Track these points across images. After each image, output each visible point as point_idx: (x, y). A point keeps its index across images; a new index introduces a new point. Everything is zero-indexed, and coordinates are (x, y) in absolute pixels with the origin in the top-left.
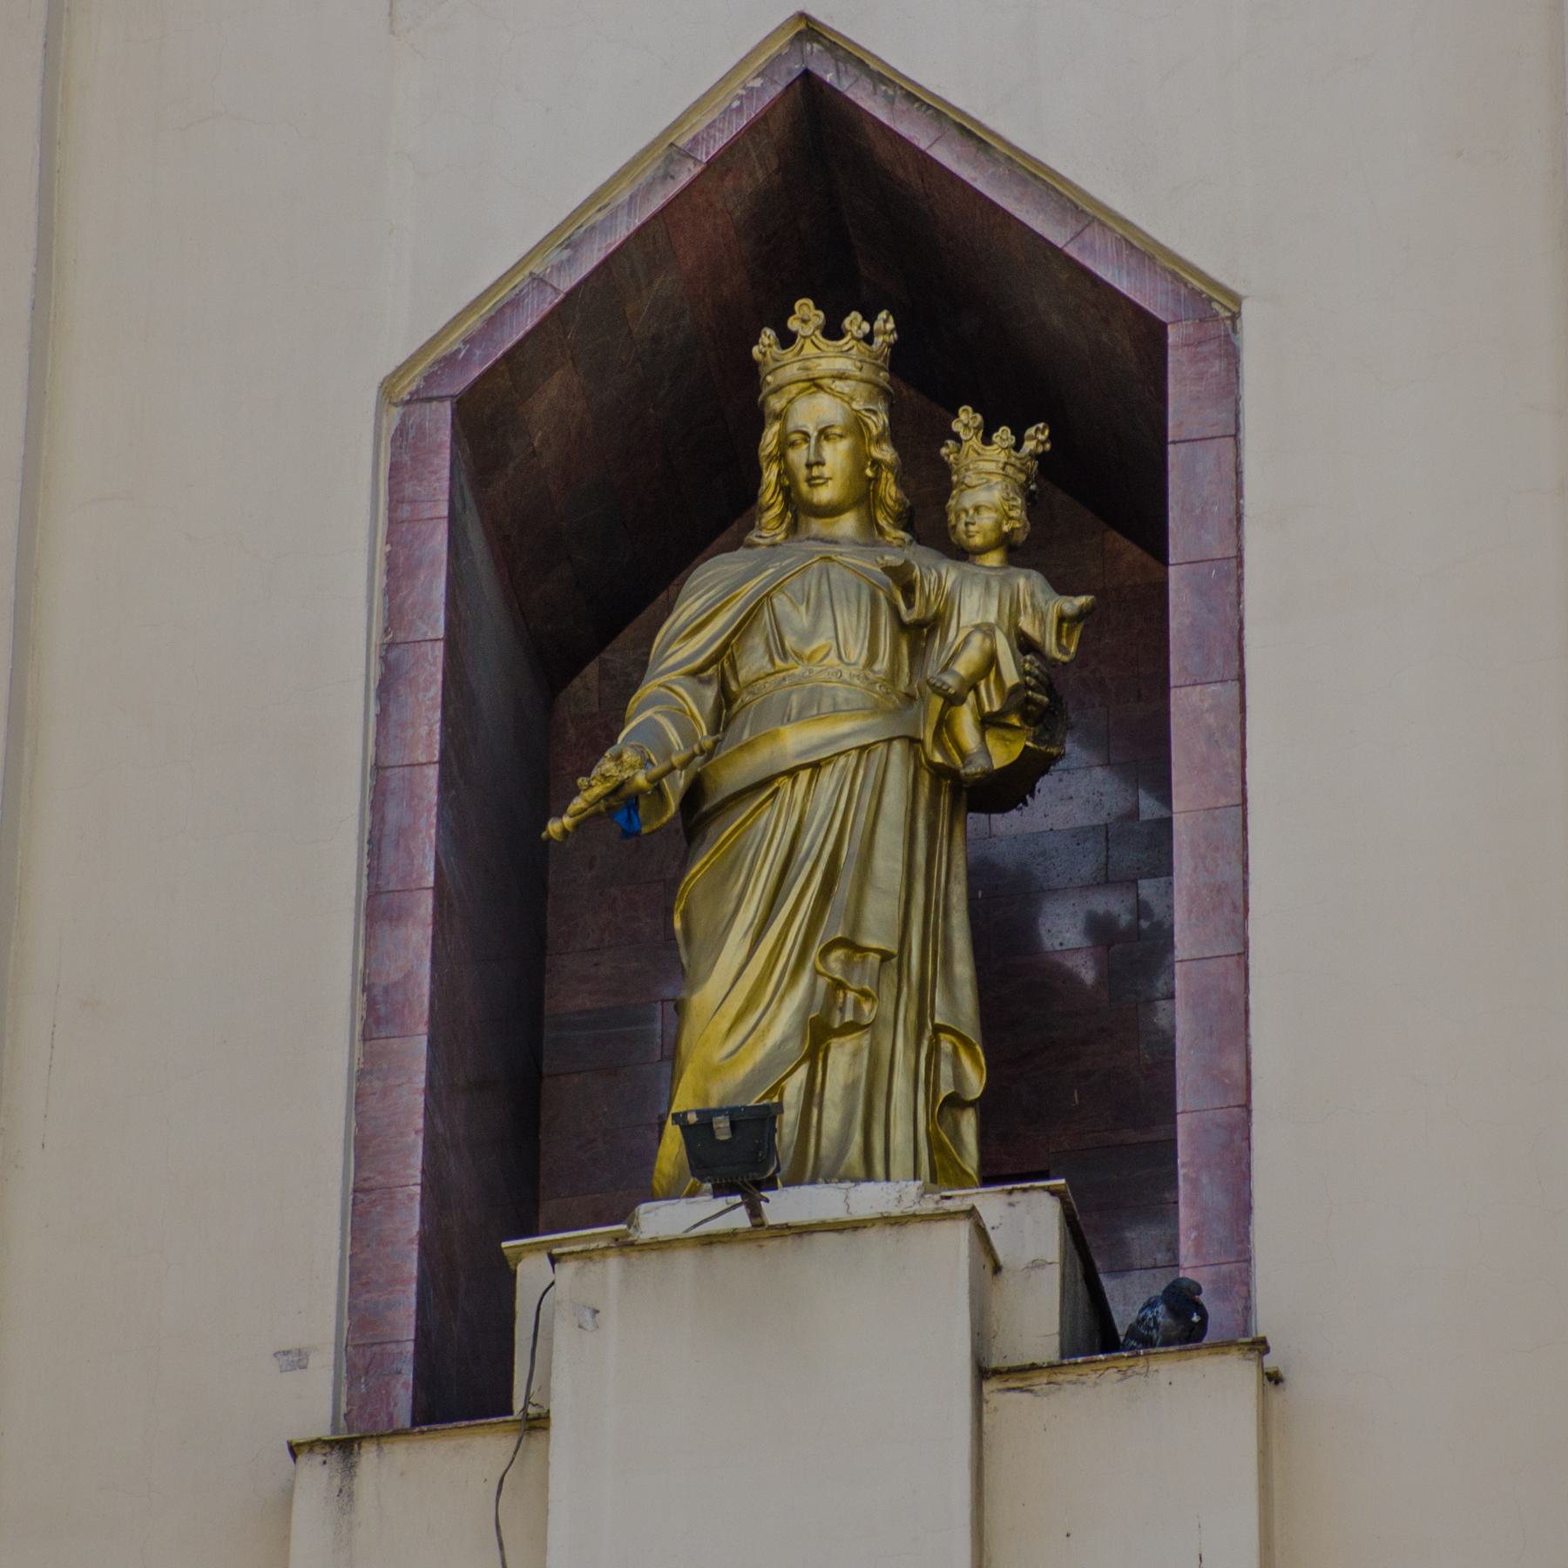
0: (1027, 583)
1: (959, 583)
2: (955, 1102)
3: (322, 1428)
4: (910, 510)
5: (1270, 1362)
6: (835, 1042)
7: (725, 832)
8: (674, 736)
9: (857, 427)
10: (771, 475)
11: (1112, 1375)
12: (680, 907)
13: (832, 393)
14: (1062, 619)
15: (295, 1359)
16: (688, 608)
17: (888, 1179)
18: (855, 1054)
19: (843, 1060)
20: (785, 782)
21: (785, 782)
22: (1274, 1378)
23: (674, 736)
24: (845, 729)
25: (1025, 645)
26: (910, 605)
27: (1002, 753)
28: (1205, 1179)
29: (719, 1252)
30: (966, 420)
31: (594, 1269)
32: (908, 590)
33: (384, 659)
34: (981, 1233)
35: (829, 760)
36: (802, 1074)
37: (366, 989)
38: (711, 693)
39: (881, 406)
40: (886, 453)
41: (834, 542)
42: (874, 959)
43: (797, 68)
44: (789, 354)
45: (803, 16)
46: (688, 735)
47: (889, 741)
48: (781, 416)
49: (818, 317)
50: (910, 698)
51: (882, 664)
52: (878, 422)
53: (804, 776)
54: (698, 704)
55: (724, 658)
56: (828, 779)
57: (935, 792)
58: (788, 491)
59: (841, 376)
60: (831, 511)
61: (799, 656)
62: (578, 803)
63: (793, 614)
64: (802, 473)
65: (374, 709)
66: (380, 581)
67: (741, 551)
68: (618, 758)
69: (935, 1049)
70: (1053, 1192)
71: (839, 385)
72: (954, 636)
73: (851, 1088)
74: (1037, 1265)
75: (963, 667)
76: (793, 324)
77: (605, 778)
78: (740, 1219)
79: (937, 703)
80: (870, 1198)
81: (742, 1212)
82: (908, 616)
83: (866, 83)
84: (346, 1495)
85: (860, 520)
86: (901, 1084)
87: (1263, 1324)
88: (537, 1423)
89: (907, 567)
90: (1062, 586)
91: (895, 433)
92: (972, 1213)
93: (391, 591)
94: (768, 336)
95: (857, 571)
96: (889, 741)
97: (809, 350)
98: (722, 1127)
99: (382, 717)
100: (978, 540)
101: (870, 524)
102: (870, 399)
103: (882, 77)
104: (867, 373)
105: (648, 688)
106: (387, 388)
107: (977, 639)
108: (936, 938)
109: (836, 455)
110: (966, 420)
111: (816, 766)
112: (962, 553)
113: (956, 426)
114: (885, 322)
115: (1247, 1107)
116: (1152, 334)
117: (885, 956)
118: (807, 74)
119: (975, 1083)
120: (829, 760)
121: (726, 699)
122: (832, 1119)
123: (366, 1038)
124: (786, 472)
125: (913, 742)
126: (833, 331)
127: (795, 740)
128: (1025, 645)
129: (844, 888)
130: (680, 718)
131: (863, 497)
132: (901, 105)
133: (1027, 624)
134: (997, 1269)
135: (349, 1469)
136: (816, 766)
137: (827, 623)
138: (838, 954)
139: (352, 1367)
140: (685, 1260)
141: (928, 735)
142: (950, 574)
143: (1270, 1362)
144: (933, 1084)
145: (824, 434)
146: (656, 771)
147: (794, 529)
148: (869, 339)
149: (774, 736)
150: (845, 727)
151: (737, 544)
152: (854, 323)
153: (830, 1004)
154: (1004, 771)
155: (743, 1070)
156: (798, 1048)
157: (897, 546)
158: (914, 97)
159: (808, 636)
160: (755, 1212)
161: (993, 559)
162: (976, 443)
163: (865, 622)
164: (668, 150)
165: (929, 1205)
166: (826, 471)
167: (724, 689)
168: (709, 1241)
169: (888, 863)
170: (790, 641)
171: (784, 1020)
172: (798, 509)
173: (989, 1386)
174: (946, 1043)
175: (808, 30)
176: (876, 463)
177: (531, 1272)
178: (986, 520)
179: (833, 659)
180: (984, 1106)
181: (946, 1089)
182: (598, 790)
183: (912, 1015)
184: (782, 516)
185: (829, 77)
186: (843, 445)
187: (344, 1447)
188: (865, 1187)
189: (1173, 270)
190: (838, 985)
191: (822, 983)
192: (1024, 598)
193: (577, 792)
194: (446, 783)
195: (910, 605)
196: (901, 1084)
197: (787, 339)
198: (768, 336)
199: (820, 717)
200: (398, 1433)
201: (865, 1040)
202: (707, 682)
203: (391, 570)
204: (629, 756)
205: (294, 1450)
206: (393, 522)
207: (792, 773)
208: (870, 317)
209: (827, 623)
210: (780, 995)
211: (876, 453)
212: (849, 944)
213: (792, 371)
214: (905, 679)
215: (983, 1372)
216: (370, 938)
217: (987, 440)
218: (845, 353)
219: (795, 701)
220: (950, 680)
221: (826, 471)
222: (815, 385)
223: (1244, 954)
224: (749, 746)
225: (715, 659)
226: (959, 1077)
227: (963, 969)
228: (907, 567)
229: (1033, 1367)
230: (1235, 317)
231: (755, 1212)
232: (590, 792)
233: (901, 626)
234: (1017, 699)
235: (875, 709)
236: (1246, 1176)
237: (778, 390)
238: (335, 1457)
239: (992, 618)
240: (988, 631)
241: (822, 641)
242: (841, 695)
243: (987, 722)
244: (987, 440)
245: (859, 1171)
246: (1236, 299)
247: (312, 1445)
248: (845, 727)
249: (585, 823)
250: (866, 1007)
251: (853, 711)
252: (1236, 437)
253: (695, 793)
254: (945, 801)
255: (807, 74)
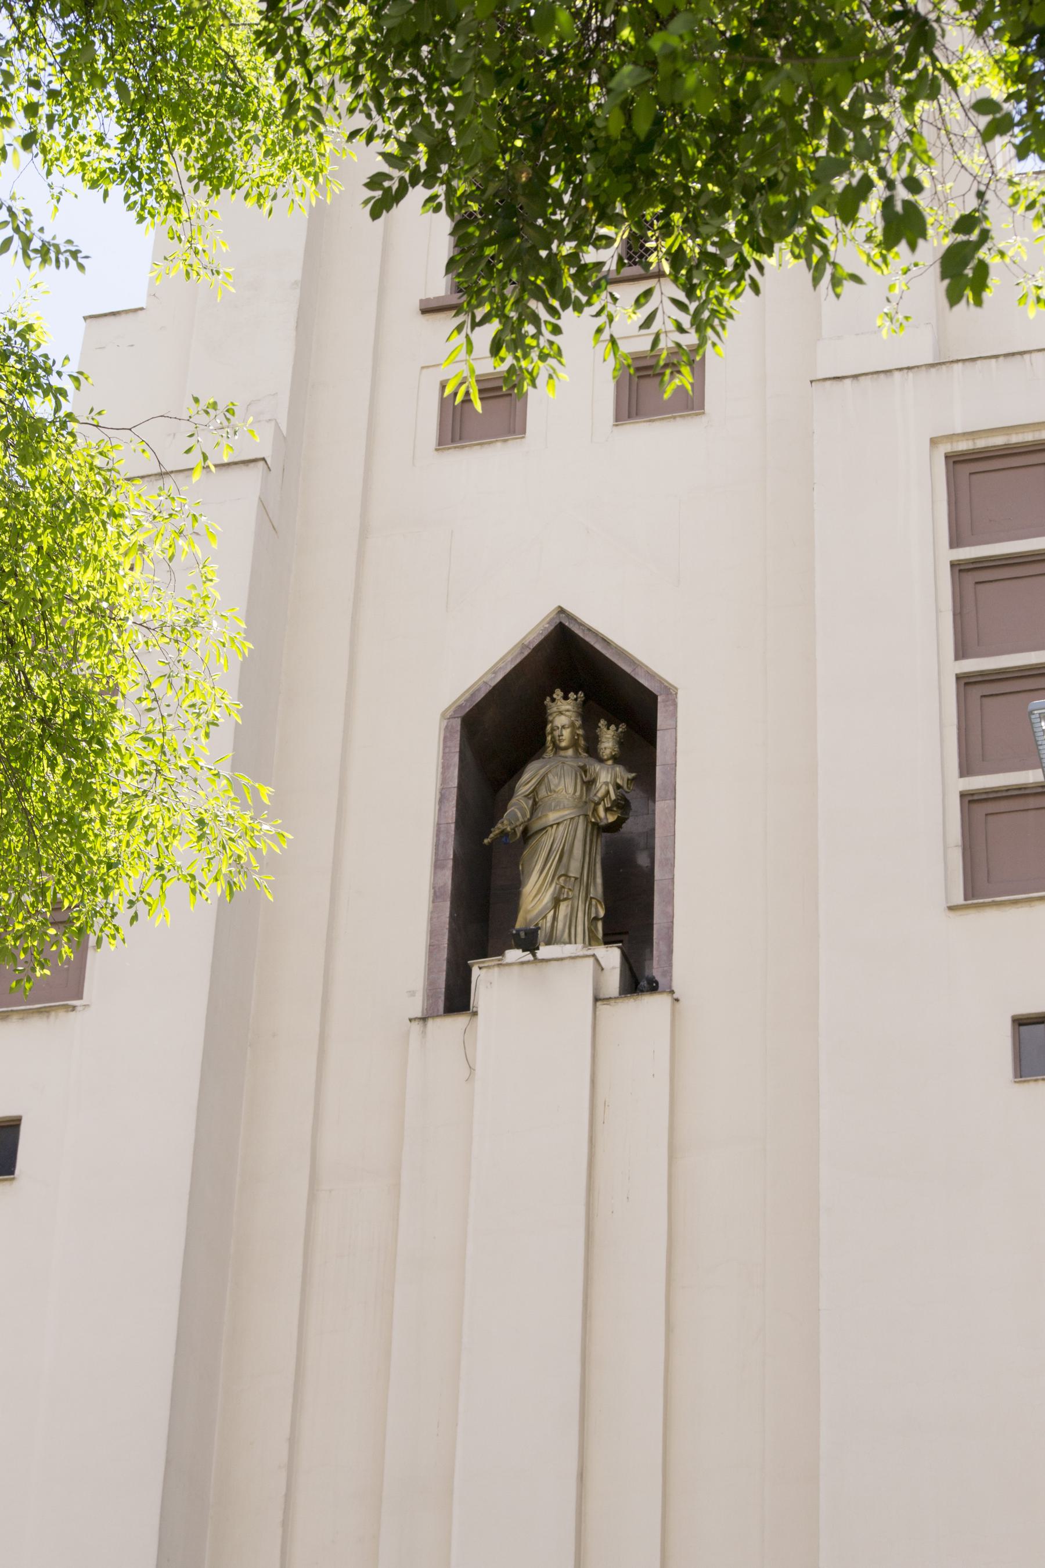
0: (619, 769)
1: (600, 769)
2: (596, 919)
3: (419, 1015)
4: (588, 748)
5: (675, 996)
6: (562, 903)
7: (533, 842)
8: (519, 815)
9: (572, 725)
10: (549, 738)
11: (632, 1000)
12: (521, 863)
13: (566, 715)
14: (628, 780)
15: (412, 994)
16: (525, 777)
17: (576, 943)
18: (567, 906)
19: (564, 908)
20: (550, 829)
21: (550, 829)
22: (677, 1000)
23: (519, 815)
24: (567, 813)
25: (618, 787)
26: (586, 776)
27: (611, 818)
28: (661, 942)
29: (525, 966)
30: (602, 723)
31: (491, 971)
32: (585, 772)
33: (441, 793)
34: (597, 960)
35: (562, 822)
36: (552, 912)
37: (434, 888)
38: (531, 802)
39: (579, 719)
40: (580, 732)
41: (566, 757)
42: (573, 879)
43: (558, 621)
44: (553, 704)
45: (560, 607)
46: (524, 815)
47: (579, 816)
48: (552, 722)
49: (561, 694)
50: (586, 802)
51: (578, 793)
52: (578, 723)
53: (555, 827)
54: (527, 805)
55: (535, 791)
56: (561, 828)
57: (592, 829)
58: (554, 742)
59: (568, 711)
60: (566, 748)
61: (555, 791)
62: (492, 835)
63: (553, 780)
64: (557, 738)
65: (437, 807)
66: (440, 770)
67: (541, 760)
68: (502, 822)
69: (590, 904)
70: (619, 947)
71: (567, 713)
72: (598, 785)
73: (566, 916)
74: (614, 968)
75: (600, 794)
76: (555, 696)
77: (499, 829)
78: (530, 957)
79: (593, 805)
80: (569, 950)
81: (530, 956)
82: (585, 779)
83: (577, 626)
84: (424, 1032)
85: (574, 751)
86: (580, 914)
87: (674, 988)
88: (475, 1014)
89: (585, 766)
90: (630, 771)
91: (583, 726)
92: (594, 955)
93: (443, 773)
94: (548, 699)
95: (572, 766)
96: (579, 816)
97: (559, 703)
98: (522, 934)
99: (440, 810)
100: (605, 757)
101: (576, 752)
102: (577, 717)
103: (581, 624)
104: (575, 709)
105: (514, 801)
106: (443, 714)
107: (604, 786)
108: (591, 872)
109: (566, 733)
110: (602, 723)
111: (558, 824)
112: (601, 761)
113: (600, 725)
114: (581, 694)
115: (672, 922)
116: (654, 698)
117: (576, 879)
118: (561, 623)
119: (602, 913)
120: (562, 822)
121: (535, 803)
122: (560, 925)
123: (433, 902)
124: (553, 738)
125: (586, 816)
126: (566, 698)
127: (552, 817)
128: (618, 787)
129: (565, 860)
130: (522, 809)
131: (574, 744)
132: (586, 632)
133: (619, 781)
134: (602, 969)
135: (425, 1026)
136: (558, 824)
137: (563, 782)
138: (562, 878)
139: (428, 996)
140: (516, 968)
141: (590, 814)
142: (598, 767)
143: (675, 996)
144: (589, 914)
145: (563, 727)
146: (513, 826)
147: (556, 753)
148: (576, 700)
149: (546, 815)
150: (567, 812)
151: (538, 758)
152: (572, 695)
153: (560, 892)
154: (612, 823)
155: (535, 912)
156: (550, 905)
157: (585, 759)
158: (590, 630)
159: (557, 785)
160: (534, 955)
161: (610, 762)
162: (605, 729)
163: (573, 782)
164: (523, 646)
165: (581, 953)
166: (564, 738)
167: (534, 800)
168: (523, 963)
169: (578, 851)
170: (552, 787)
171: (547, 898)
172: (557, 748)
173: (599, 1003)
174: (594, 902)
175: (561, 611)
176: (578, 735)
177: (475, 972)
178: (608, 751)
179: (564, 792)
180: (605, 920)
181: (593, 915)
182: (497, 832)
183: (584, 894)
184: (552, 750)
185: (567, 624)
186: (568, 730)
187: (424, 1019)
188: (568, 946)
189: (661, 681)
190: (563, 887)
191: (558, 886)
192: (618, 774)
193: (491, 832)
194: (457, 828)
195: (586, 776)
196: (580, 914)
197: (553, 700)
198: (548, 699)
199: (560, 810)
200: (438, 1016)
201: (570, 902)
202: (530, 798)
203: (443, 767)
204: (505, 822)
205: (410, 1020)
206: (444, 753)
207: (552, 826)
208: (576, 693)
209: (563, 782)
210: (546, 890)
211: (578, 732)
212: (566, 875)
213: (555, 709)
214: (584, 797)
215: (596, 999)
216: (435, 873)
217: (608, 729)
218: (569, 704)
219: (553, 804)
220: (596, 799)
221: (564, 738)
222: (561, 713)
223: (673, 878)
224: (540, 818)
225: (532, 792)
226: (597, 911)
227: (599, 880)
228: (585, 766)
229: (610, 998)
230: (676, 694)
231: (534, 955)
232: (495, 832)
233: (583, 782)
234: (615, 803)
235: (575, 807)
236: (672, 942)
237: (551, 714)
238: (421, 1022)
239: (609, 780)
240: (607, 783)
241: (561, 787)
242: (566, 802)
243: (607, 810)
244: (608, 729)
245: (567, 940)
246: (676, 689)
247: (415, 1019)
248: (567, 812)
249: (494, 840)
250: (570, 893)
251: (568, 808)
252: (676, 729)
253: (525, 831)
254: (595, 832)
255: (561, 623)
